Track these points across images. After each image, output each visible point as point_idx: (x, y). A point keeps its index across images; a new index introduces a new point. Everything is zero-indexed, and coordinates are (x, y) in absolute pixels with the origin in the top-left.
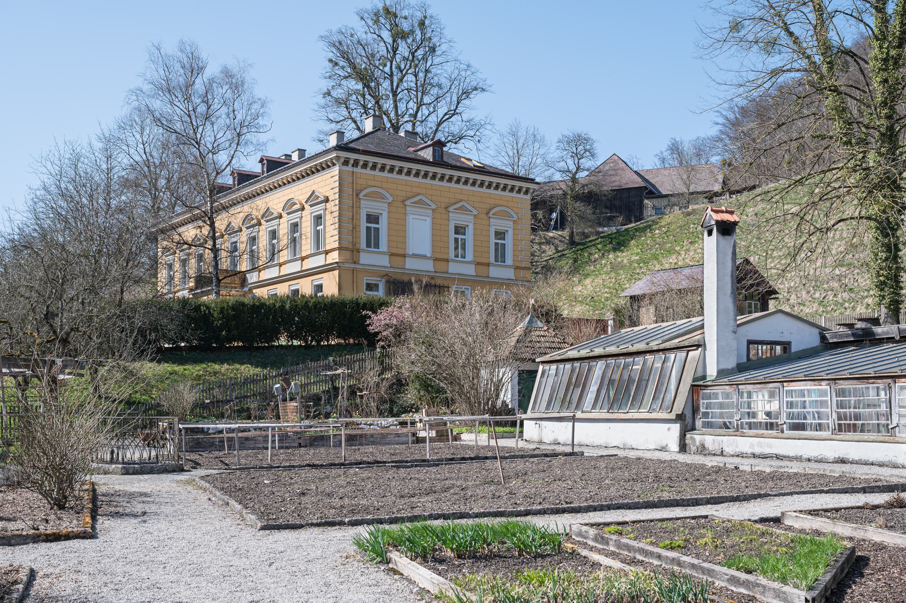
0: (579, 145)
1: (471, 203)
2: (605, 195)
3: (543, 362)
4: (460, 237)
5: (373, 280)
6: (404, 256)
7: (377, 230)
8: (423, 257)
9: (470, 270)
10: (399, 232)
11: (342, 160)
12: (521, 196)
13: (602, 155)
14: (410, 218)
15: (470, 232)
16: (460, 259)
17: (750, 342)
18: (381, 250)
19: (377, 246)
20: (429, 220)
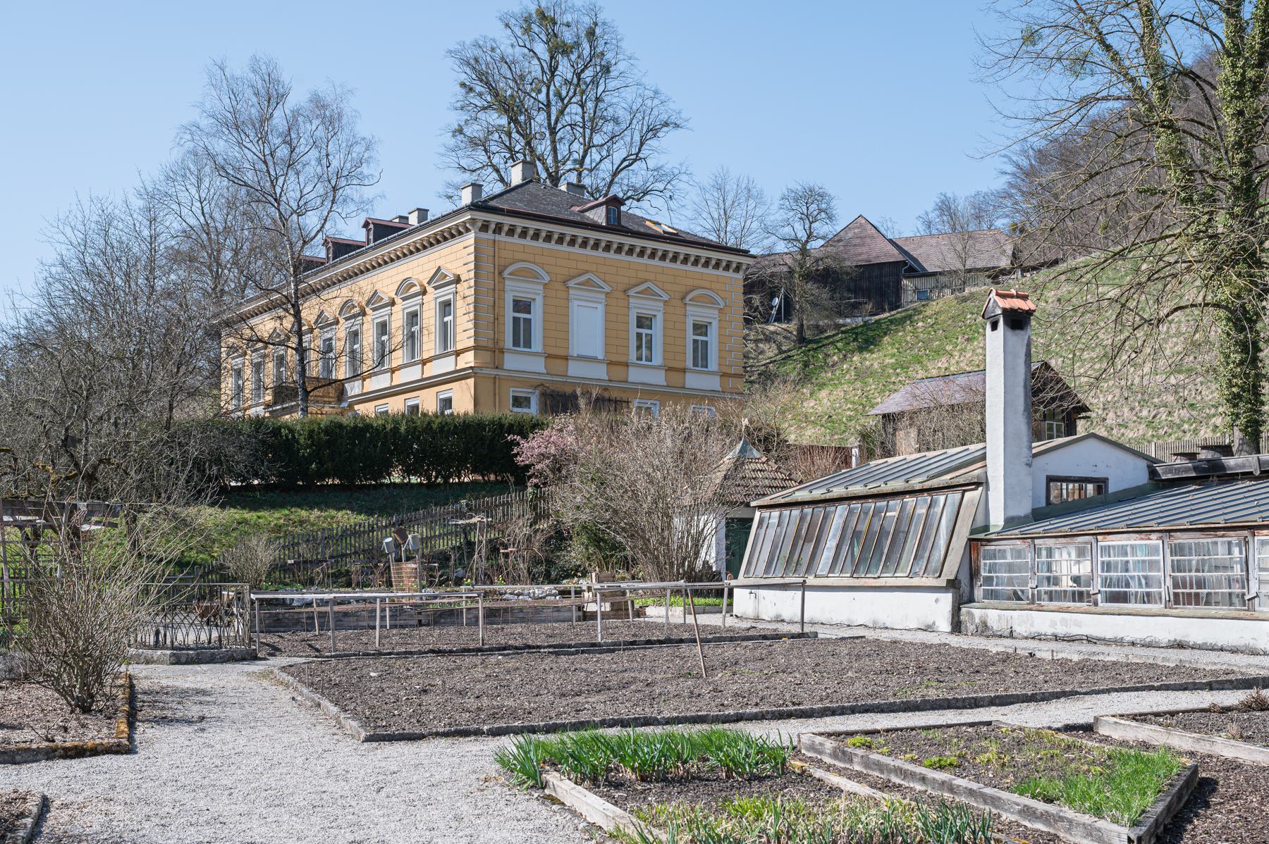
0: (811, 203)
1: (660, 284)
2: (848, 274)
3: (760, 507)
4: (644, 331)
5: (522, 392)
6: (566, 358)
7: (528, 321)
8: (593, 359)
9: (658, 378)
10: (559, 324)
11: (479, 224)
12: (730, 274)
13: (844, 217)
14: (574, 305)
15: (658, 325)
16: (644, 362)
17: (1050, 479)
18: (533, 349)
19: (528, 344)
20: (601, 307)
